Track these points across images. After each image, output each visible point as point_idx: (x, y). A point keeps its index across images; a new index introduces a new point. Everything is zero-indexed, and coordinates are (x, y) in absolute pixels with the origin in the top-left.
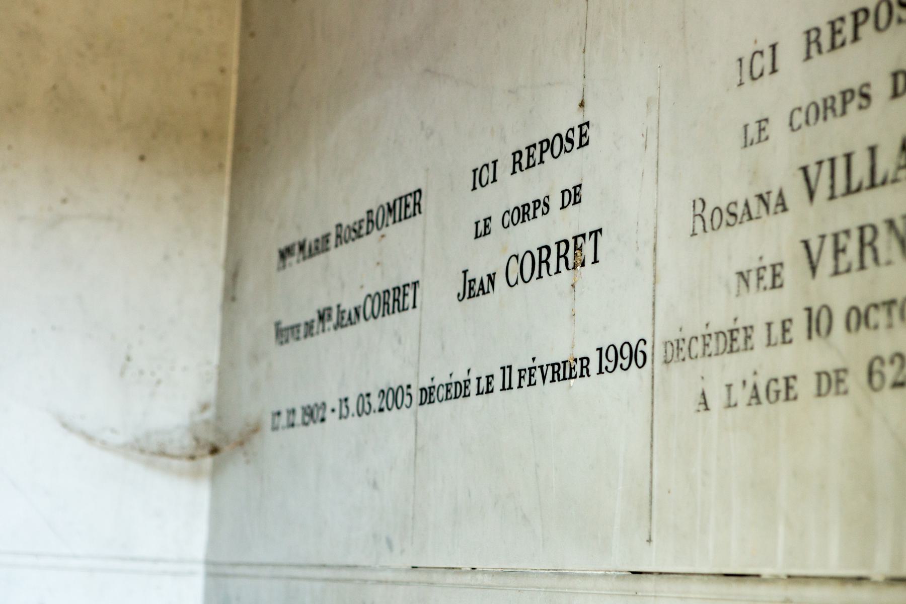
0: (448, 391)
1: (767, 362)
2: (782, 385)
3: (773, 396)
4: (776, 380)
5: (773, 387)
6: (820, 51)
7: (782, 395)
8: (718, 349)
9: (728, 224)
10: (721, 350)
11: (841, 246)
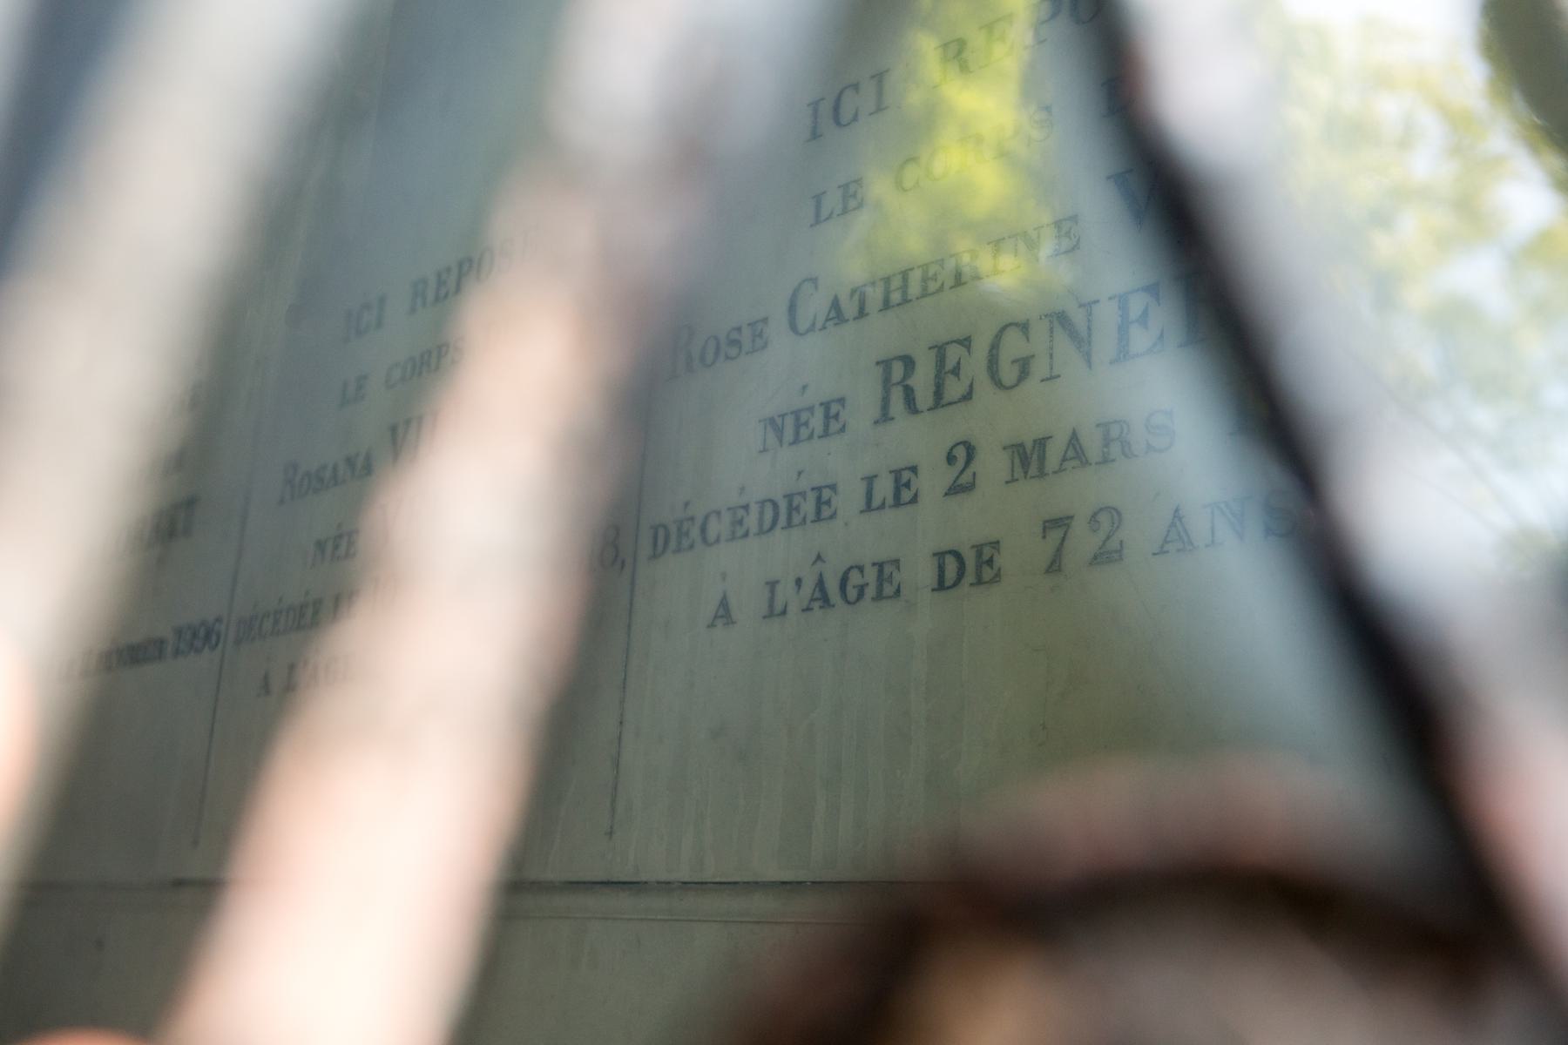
0: (276, 622)
1: (856, 537)
2: (871, 575)
3: (852, 593)
4: (861, 569)
5: (855, 578)
6: (424, 304)
7: (870, 591)
8: (761, 520)
9: (728, 358)
10: (767, 525)
11: (795, 504)
